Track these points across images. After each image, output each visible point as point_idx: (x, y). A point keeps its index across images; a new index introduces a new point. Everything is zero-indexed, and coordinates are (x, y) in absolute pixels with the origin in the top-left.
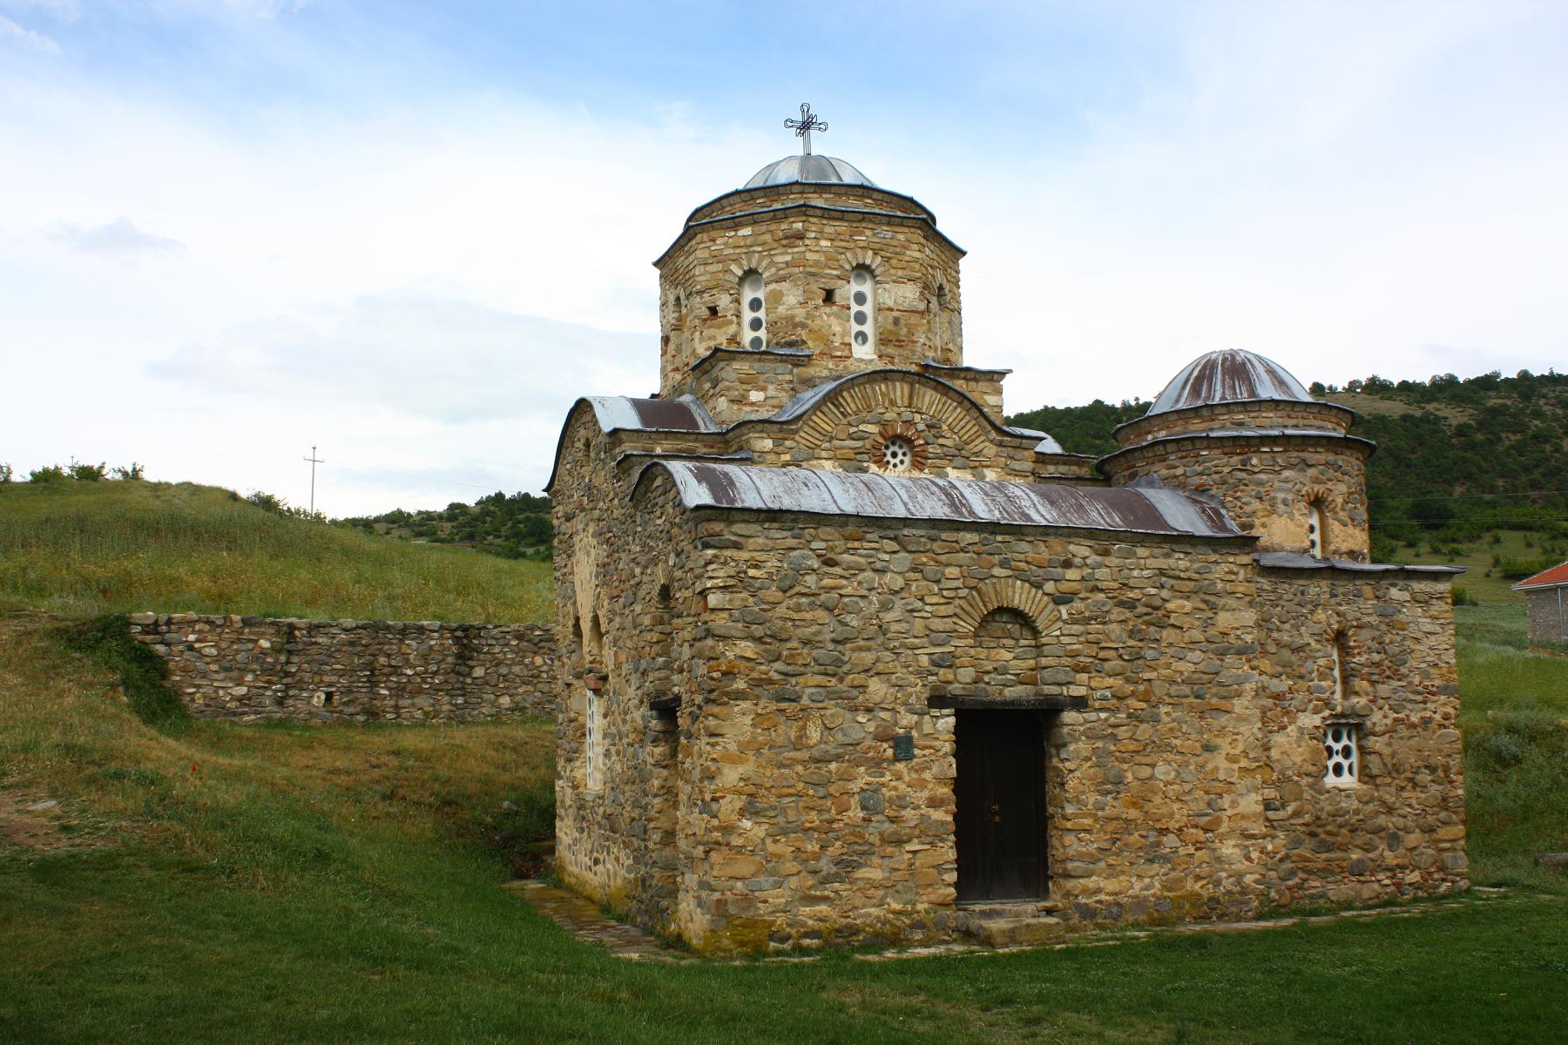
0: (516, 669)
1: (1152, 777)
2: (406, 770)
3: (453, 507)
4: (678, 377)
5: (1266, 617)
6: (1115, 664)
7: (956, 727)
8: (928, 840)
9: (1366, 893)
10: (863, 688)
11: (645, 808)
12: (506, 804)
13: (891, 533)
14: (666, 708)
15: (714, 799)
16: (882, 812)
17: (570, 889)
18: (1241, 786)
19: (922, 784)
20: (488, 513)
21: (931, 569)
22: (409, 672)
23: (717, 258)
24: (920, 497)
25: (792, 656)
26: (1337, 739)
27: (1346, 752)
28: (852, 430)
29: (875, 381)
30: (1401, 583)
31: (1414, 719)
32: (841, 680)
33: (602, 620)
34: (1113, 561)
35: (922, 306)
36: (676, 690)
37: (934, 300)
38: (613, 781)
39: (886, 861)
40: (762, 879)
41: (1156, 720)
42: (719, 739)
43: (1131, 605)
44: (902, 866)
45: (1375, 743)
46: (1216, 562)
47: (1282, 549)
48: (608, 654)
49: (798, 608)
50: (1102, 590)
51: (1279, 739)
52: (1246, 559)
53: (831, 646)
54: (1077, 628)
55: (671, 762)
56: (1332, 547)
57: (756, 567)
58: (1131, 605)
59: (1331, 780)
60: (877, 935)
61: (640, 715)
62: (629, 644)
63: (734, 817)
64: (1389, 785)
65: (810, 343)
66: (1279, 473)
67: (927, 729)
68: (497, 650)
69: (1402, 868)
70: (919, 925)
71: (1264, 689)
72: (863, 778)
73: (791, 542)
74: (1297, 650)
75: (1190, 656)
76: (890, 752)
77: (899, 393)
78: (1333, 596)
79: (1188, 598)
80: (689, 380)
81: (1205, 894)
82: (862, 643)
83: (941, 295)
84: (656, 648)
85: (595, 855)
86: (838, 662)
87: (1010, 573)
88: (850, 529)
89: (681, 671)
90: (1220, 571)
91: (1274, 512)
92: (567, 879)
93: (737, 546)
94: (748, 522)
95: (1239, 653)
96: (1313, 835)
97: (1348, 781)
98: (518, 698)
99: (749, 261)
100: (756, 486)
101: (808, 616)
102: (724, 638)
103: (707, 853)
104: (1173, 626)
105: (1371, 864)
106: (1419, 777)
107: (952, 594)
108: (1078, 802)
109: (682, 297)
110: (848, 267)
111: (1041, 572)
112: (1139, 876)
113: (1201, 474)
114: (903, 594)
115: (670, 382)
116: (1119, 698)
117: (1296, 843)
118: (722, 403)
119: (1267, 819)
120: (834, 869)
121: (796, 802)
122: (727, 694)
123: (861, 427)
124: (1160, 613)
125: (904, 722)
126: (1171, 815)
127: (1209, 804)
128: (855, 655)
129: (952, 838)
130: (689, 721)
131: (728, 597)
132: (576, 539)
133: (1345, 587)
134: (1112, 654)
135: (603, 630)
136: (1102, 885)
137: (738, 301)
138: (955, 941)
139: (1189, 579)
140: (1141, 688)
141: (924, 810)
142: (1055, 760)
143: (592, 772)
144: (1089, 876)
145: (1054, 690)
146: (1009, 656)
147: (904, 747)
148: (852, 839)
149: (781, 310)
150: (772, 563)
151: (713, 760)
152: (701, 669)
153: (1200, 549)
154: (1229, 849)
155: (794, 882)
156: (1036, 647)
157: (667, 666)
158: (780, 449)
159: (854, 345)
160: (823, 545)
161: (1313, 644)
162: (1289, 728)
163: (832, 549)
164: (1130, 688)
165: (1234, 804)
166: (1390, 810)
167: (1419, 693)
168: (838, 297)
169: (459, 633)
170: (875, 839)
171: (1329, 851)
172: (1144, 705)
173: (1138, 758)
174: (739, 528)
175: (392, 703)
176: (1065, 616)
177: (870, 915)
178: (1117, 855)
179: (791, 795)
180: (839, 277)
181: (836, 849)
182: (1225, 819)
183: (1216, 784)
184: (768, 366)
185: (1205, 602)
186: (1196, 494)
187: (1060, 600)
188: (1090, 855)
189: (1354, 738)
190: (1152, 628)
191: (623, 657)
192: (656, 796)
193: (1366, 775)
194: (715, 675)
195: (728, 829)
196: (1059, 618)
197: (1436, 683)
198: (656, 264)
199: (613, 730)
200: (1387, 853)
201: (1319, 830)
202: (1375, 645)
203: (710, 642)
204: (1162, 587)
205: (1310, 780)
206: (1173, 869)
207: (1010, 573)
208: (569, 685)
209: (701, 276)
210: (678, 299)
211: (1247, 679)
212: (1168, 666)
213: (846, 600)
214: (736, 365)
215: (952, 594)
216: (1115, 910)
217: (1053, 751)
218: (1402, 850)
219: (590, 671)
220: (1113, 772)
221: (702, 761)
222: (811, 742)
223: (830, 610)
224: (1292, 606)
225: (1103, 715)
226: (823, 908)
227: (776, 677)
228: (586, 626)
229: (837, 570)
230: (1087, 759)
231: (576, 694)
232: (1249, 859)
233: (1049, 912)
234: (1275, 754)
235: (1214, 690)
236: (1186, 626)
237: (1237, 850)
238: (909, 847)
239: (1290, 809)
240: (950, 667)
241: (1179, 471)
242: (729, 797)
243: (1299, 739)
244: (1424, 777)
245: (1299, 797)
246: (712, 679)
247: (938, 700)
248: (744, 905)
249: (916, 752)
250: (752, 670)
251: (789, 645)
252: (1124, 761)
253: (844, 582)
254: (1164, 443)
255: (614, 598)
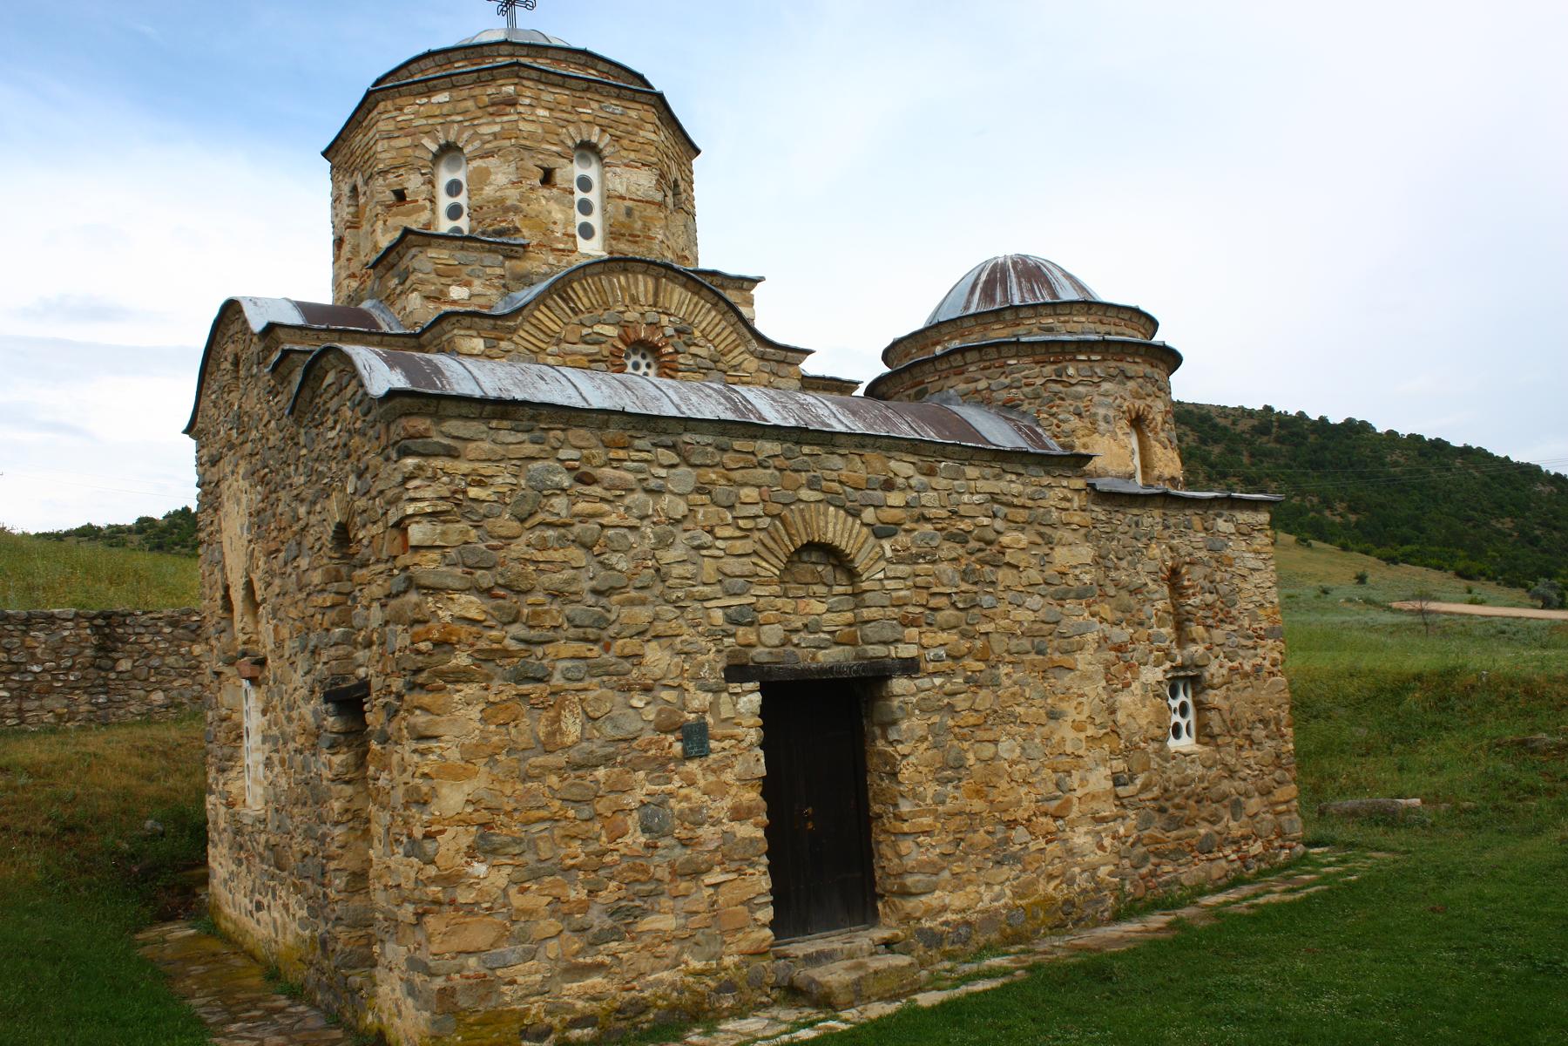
0: (171, 660)
1: (995, 757)
2: (15, 789)
3: (141, 520)
4: (354, 284)
5: (1103, 552)
6: (948, 614)
7: (762, 707)
8: (734, 866)
9: (1216, 874)
10: (637, 658)
11: (322, 840)
12: (149, 824)
13: (668, 440)
14: (348, 700)
15: (429, 836)
16: (670, 834)
17: (227, 939)
18: (1089, 758)
19: (722, 789)
20: (175, 526)
21: (721, 490)
22: (36, 669)
23: (404, 130)
24: (694, 399)
25: (536, 615)
26: (1174, 695)
27: (1183, 710)
28: (585, 331)
29: (611, 271)
30: (1226, 513)
31: (1247, 667)
32: (607, 648)
33: (257, 585)
34: (940, 482)
35: (659, 197)
36: (361, 672)
37: (670, 194)
38: (277, 801)
39: (680, 903)
40: (505, 948)
41: (996, 683)
42: (433, 744)
43: (961, 538)
44: (702, 907)
45: (1214, 697)
46: (1049, 486)
47: (1107, 474)
48: (266, 631)
49: (543, 546)
50: (928, 520)
51: (1124, 699)
52: (1079, 483)
53: (591, 599)
54: (903, 569)
55: (357, 773)
56: (1156, 473)
57: (480, 484)
58: (961, 538)
59: (1173, 744)
60: (673, 1008)
61: (310, 709)
62: (293, 613)
63: (461, 860)
64: (1228, 744)
65: (525, 232)
66: (1097, 385)
67: (726, 711)
68: (147, 639)
69: (1245, 838)
70: (728, 987)
71: (1106, 639)
72: (643, 787)
73: (530, 449)
74: (1135, 592)
75: (1029, 602)
76: (678, 747)
77: (641, 288)
78: (1167, 527)
79: (1022, 530)
80: (369, 283)
81: (1060, 898)
82: (633, 594)
83: (676, 194)
84: (332, 615)
85: (257, 897)
86: (602, 622)
87: (820, 496)
88: (612, 433)
89: (369, 644)
90: (1053, 497)
91: (1095, 431)
92: (223, 924)
93: (452, 454)
94: (466, 418)
95: (1079, 597)
96: (1162, 810)
97: (1186, 743)
98: (174, 693)
99: (447, 133)
100: (469, 373)
101: (557, 556)
102: (434, 590)
103: (419, 916)
104: (1009, 564)
105: (1217, 838)
106: (1255, 733)
107: (749, 524)
108: (915, 796)
109: (360, 183)
110: (570, 143)
111: (858, 495)
112: (987, 884)
113: (1009, 387)
114: (686, 525)
115: (344, 293)
116: (955, 658)
117: (1146, 822)
118: (414, 300)
119: (1117, 797)
120: (609, 923)
121: (550, 830)
122: (441, 674)
123: (597, 328)
124: (995, 548)
125: (696, 704)
126: (1019, 803)
127: (1057, 785)
128: (625, 611)
129: (765, 860)
130: (382, 717)
131: (439, 528)
132: (224, 486)
133: (1177, 517)
134: (943, 601)
135: (259, 598)
136: (949, 901)
137: (431, 183)
138: (775, 1001)
139: (1023, 507)
140: (979, 644)
141: (728, 825)
142: (880, 744)
143: (250, 785)
144: (932, 892)
145: (879, 651)
146: (822, 608)
147: (696, 739)
148: (632, 875)
149: (488, 191)
150: (503, 479)
151: (424, 775)
152: (400, 638)
153: (1033, 470)
154: (1081, 838)
155: (553, 948)
156: (853, 595)
157: (347, 639)
158: (494, 352)
159: (579, 239)
160: (575, 454)
161: (1150, 584)
162: (1134, 685)
163: (588, 460)
164: (965, 645)
165: (1084, 781)
166: (1232, 774)
167: (1249, 637)
168: (559, 177)
169: (99, 622)
170: (663, 873)
171: (1178, 828)
172: (981, 666)
173: (980, 734)
174: (453, 426)
175: (14, 706)
176: (889, 554)
177: (661, 982)
178: (962, 860)
179: (542, 820)
180: (559, 155)
181: (610, 893)
182: (1075, 801)
183: (1064, 759)
184: (473, 255)
185: (1041, 535)
186: (1008, 408)
187: (883, 531)
188: (932, 863)
189: (1190, 693)
190: (987, 568)
191: (285, 632)
192: (337, 824)
193: (1204, 733)
194: (423, 646)
195: (451, 880)
196: (882, 557)
197: (1264, 625)
198: (325, 154)
199: (275, 731)
200: (1232, 824)
201: (1168, 804)
202: (1207, 585)
203: (413, 597)
204: (995, 516)
205: (1156, 745)
206: (1024, 870)
207: (820, 496)
208: (218, 674)
209: (385, 153)
210: (354, 189)
211: (1088, 628)
212: (1006, 615)
213: (610, 532)
214: (432, 253)
215: (749, 524)
216: (963, 931)
217: (878, 731)
218: (1244, 819)
219: (244, 654)
220: (953, 754)
221: (406, 777)
222: (569, 740)
223: (588, 547)
224: (1126, 540)
225: (938, 681)
226: (596, 981)
227: (514, 646)
228: (237, 595)
229: (596, 490)
230: (923, 739)
231: (228, 686)
232: (1101, 847)
233: (889, 945)
234: (1121, 717)
235: (1055, 643)
236: (1022, 565)
237: (1089, 838)
238: (710, 879)
239: (1138, 782)
240: (751, 624)
241: (982, 385)
242: (451, 832)
243: (1144, 697)
244: (1259, 733)
245: (1146, 768)
246: (419, 652)
247: (737, 671)
248: (482, 991)
249: (713, 744)
250: (479, 637)
251: (531, 599)
252: (963, 738)
253: (606, 507)
254: (961, 351)
255: (272, 554)
